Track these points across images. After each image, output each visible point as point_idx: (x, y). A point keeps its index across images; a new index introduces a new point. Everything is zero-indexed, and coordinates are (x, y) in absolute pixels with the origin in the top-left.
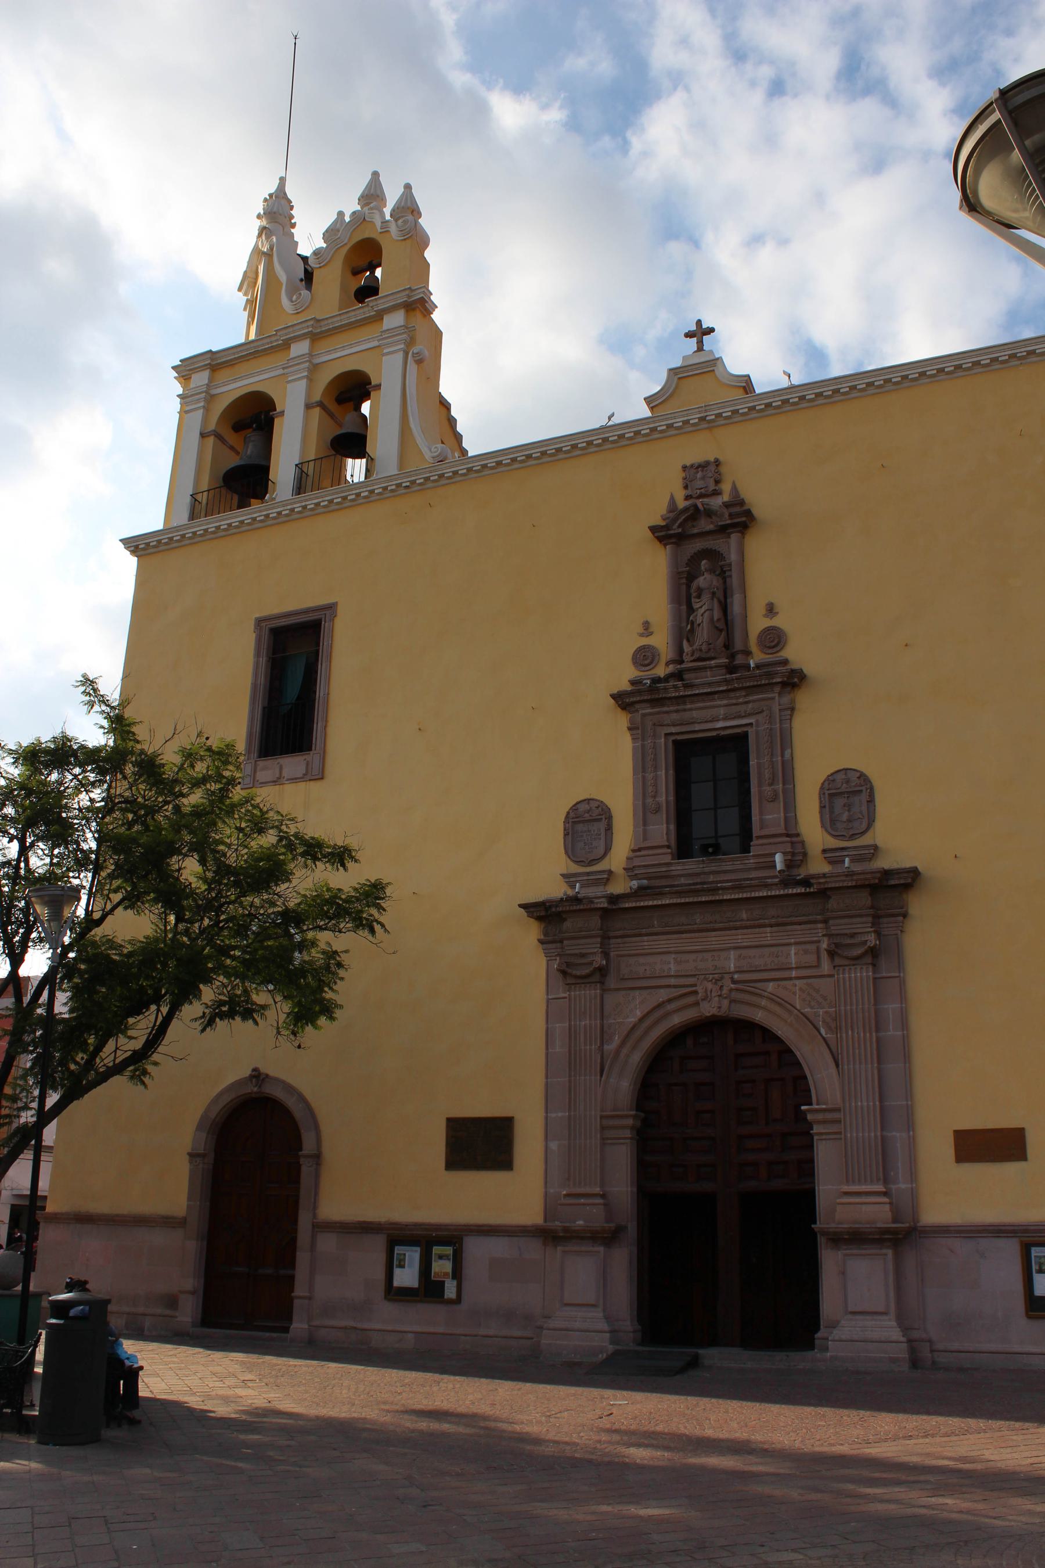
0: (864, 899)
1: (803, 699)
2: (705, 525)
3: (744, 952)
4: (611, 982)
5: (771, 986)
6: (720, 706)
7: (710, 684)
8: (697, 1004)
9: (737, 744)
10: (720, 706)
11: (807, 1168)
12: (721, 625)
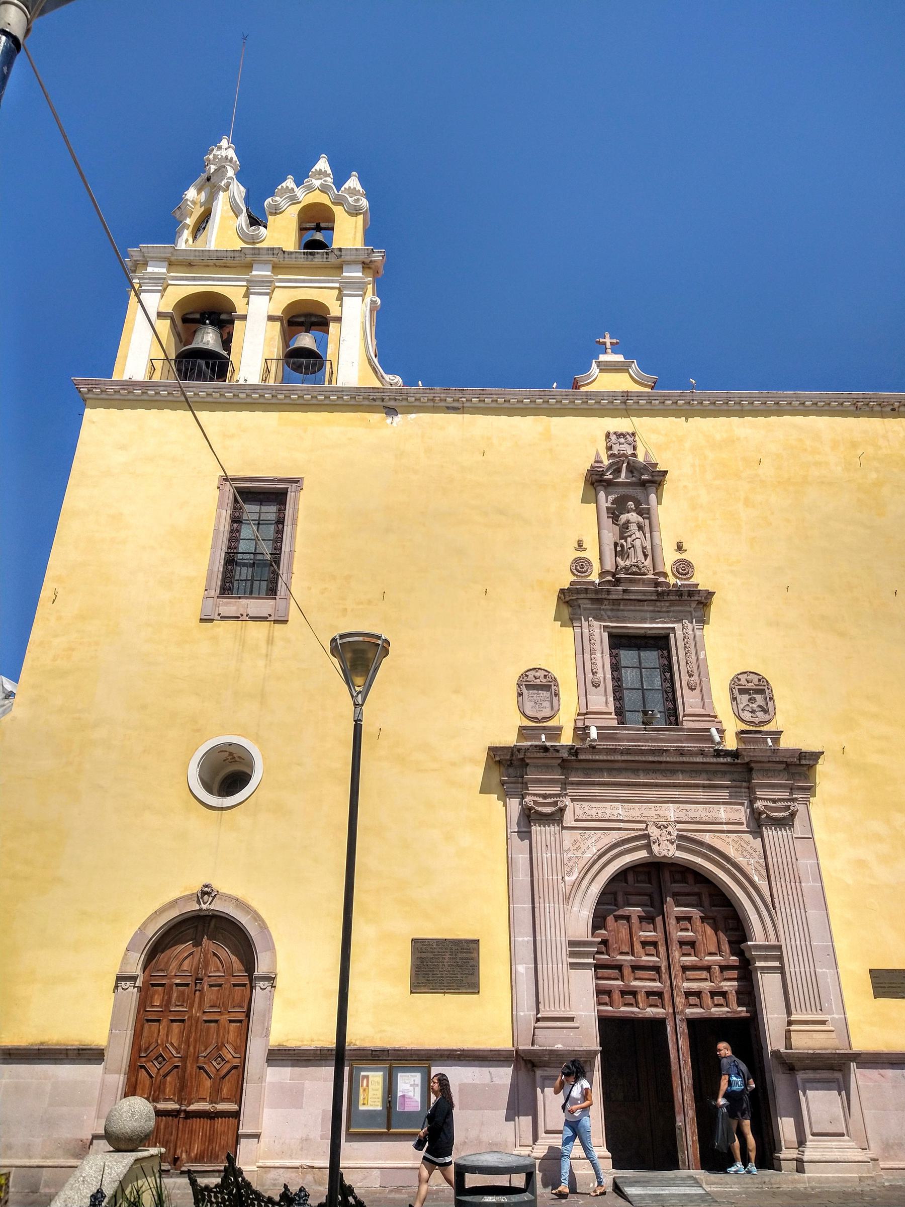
6: (647, 611)
7: (644, 593)
9: (660, 642)
10: (647, 611)
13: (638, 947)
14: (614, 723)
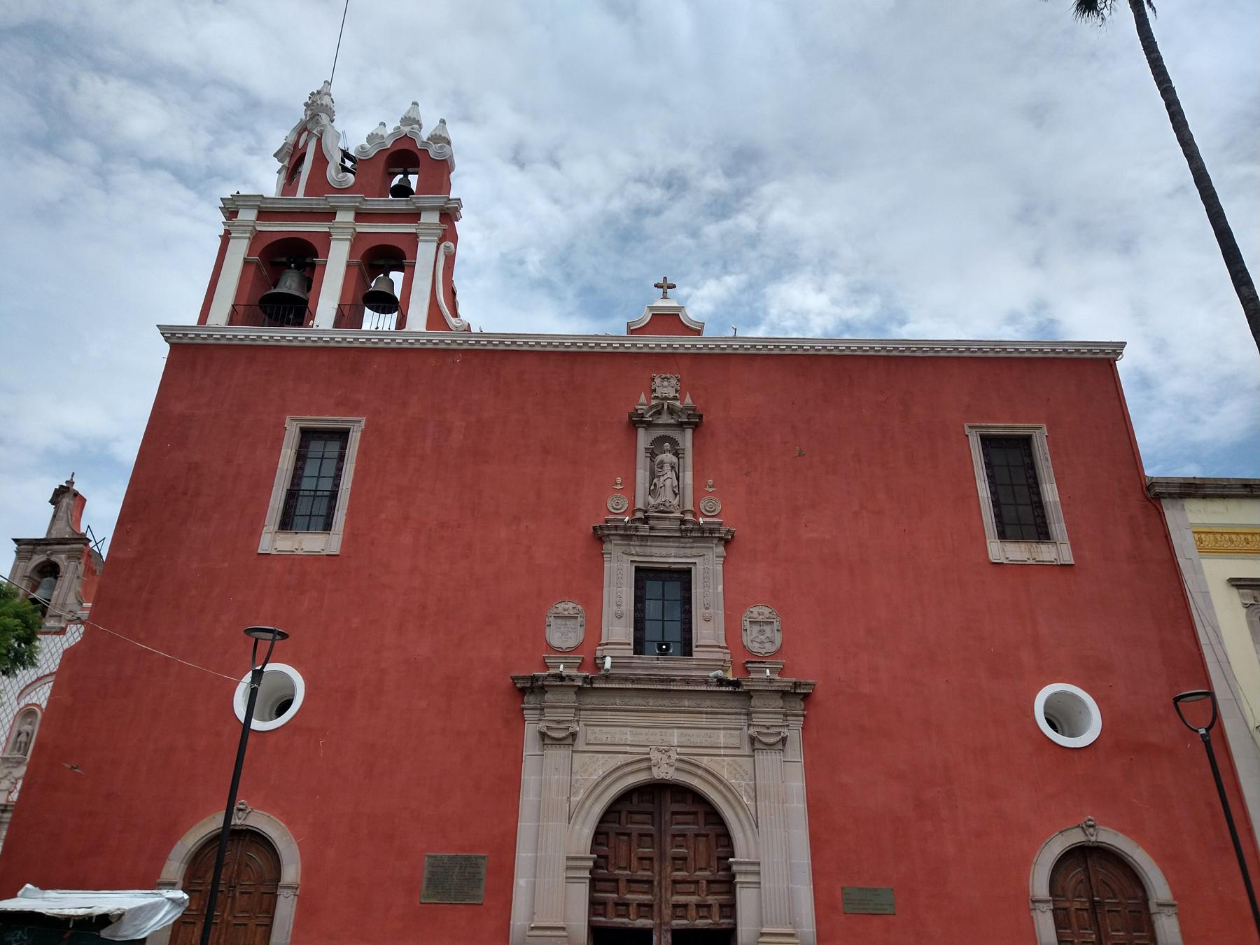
0: (571, 697)
4: (580, 744)
7: (668, 530)
8: (649, 768)
13: (635, 862)
14: (631, 653)
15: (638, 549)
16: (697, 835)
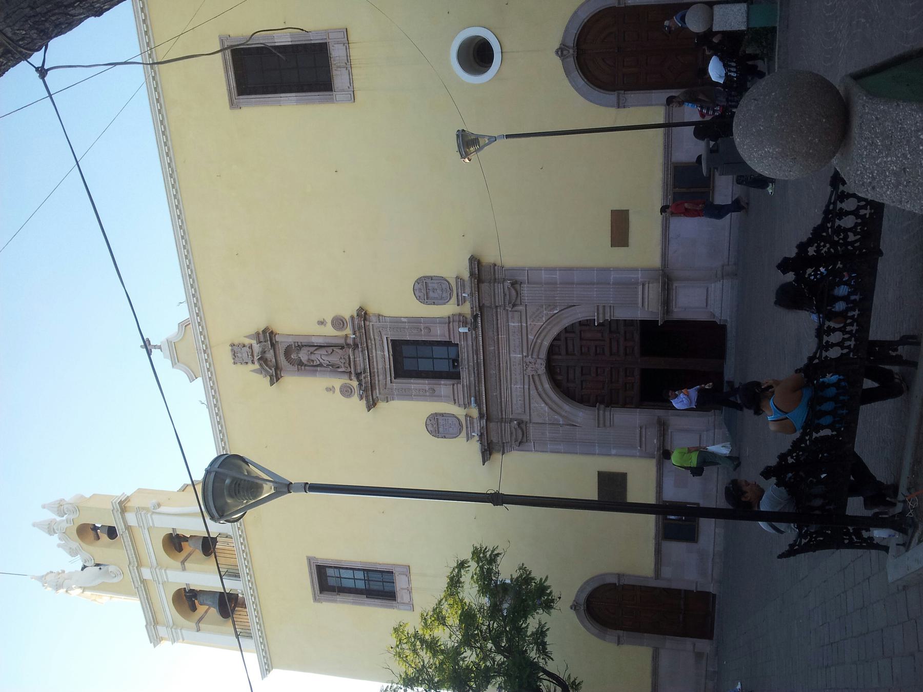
0: (485, 287)
1: (373, 309)
2: (270, 355)
3: (512, 349)
4: (526, 418)
5: (531, 337)
7: (364, 359)
9: (397, 345)
11: (628, 323)
12: (330, 350)
15: (381, 377)
16: (581, 339)
